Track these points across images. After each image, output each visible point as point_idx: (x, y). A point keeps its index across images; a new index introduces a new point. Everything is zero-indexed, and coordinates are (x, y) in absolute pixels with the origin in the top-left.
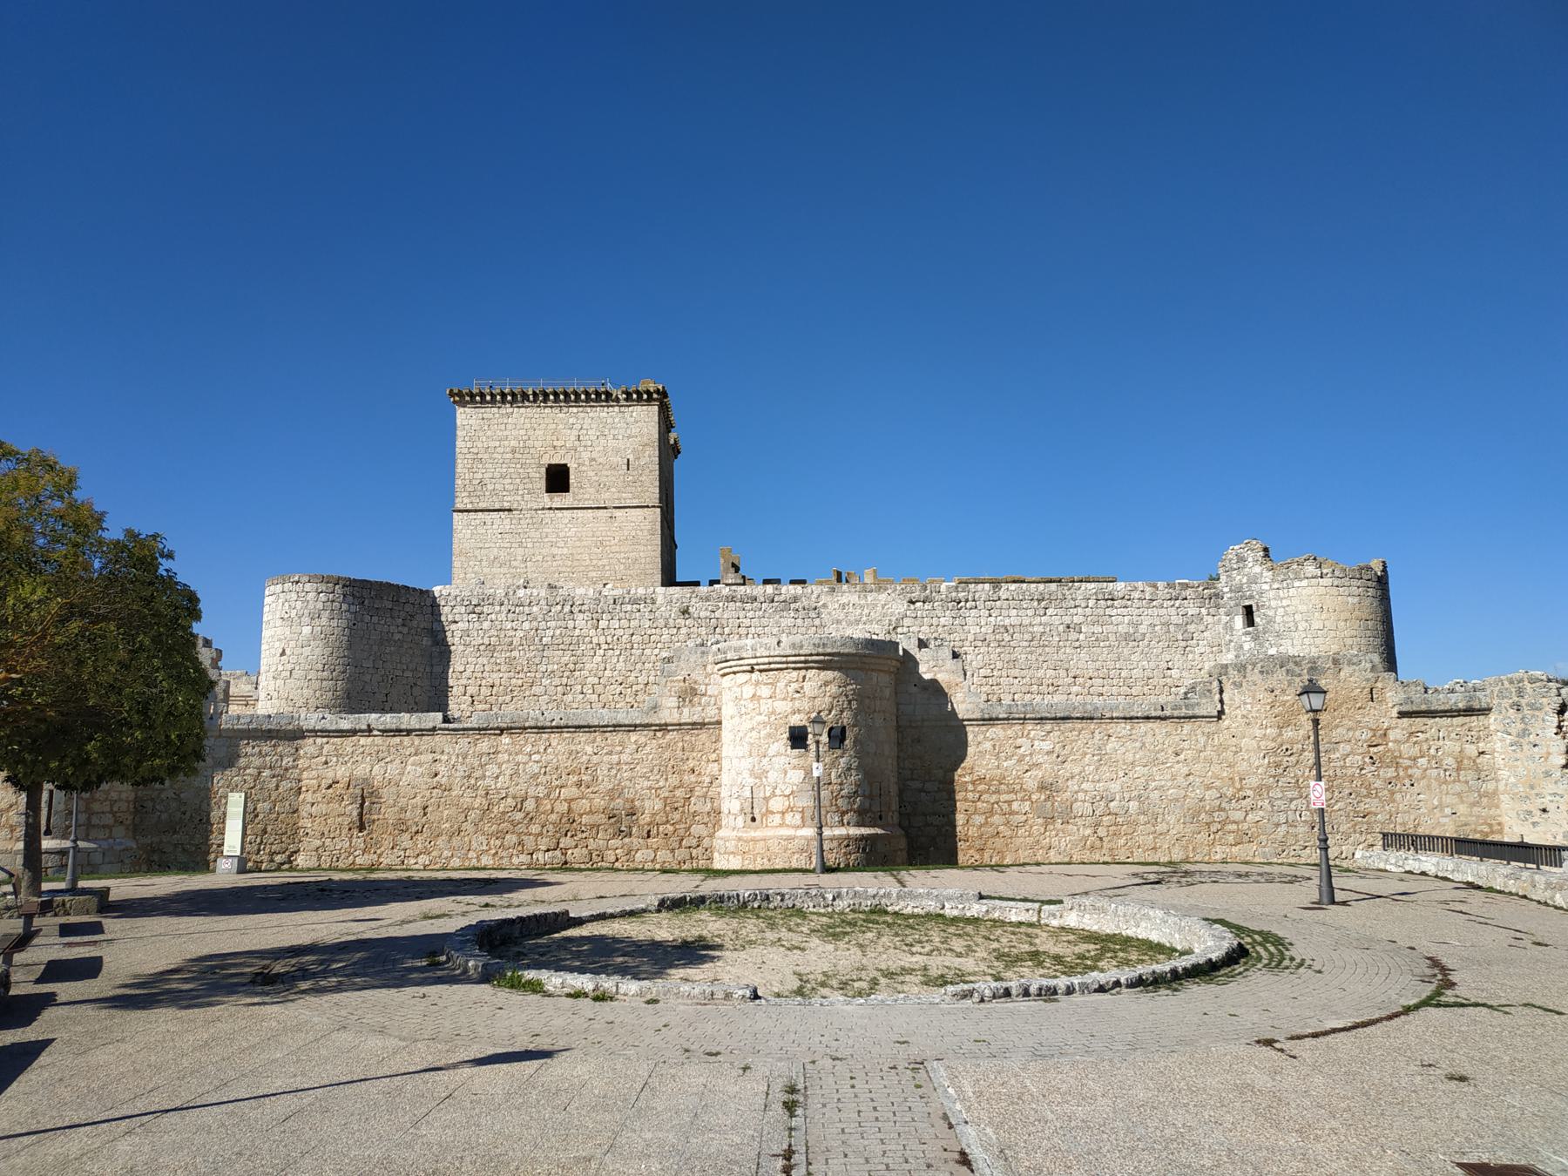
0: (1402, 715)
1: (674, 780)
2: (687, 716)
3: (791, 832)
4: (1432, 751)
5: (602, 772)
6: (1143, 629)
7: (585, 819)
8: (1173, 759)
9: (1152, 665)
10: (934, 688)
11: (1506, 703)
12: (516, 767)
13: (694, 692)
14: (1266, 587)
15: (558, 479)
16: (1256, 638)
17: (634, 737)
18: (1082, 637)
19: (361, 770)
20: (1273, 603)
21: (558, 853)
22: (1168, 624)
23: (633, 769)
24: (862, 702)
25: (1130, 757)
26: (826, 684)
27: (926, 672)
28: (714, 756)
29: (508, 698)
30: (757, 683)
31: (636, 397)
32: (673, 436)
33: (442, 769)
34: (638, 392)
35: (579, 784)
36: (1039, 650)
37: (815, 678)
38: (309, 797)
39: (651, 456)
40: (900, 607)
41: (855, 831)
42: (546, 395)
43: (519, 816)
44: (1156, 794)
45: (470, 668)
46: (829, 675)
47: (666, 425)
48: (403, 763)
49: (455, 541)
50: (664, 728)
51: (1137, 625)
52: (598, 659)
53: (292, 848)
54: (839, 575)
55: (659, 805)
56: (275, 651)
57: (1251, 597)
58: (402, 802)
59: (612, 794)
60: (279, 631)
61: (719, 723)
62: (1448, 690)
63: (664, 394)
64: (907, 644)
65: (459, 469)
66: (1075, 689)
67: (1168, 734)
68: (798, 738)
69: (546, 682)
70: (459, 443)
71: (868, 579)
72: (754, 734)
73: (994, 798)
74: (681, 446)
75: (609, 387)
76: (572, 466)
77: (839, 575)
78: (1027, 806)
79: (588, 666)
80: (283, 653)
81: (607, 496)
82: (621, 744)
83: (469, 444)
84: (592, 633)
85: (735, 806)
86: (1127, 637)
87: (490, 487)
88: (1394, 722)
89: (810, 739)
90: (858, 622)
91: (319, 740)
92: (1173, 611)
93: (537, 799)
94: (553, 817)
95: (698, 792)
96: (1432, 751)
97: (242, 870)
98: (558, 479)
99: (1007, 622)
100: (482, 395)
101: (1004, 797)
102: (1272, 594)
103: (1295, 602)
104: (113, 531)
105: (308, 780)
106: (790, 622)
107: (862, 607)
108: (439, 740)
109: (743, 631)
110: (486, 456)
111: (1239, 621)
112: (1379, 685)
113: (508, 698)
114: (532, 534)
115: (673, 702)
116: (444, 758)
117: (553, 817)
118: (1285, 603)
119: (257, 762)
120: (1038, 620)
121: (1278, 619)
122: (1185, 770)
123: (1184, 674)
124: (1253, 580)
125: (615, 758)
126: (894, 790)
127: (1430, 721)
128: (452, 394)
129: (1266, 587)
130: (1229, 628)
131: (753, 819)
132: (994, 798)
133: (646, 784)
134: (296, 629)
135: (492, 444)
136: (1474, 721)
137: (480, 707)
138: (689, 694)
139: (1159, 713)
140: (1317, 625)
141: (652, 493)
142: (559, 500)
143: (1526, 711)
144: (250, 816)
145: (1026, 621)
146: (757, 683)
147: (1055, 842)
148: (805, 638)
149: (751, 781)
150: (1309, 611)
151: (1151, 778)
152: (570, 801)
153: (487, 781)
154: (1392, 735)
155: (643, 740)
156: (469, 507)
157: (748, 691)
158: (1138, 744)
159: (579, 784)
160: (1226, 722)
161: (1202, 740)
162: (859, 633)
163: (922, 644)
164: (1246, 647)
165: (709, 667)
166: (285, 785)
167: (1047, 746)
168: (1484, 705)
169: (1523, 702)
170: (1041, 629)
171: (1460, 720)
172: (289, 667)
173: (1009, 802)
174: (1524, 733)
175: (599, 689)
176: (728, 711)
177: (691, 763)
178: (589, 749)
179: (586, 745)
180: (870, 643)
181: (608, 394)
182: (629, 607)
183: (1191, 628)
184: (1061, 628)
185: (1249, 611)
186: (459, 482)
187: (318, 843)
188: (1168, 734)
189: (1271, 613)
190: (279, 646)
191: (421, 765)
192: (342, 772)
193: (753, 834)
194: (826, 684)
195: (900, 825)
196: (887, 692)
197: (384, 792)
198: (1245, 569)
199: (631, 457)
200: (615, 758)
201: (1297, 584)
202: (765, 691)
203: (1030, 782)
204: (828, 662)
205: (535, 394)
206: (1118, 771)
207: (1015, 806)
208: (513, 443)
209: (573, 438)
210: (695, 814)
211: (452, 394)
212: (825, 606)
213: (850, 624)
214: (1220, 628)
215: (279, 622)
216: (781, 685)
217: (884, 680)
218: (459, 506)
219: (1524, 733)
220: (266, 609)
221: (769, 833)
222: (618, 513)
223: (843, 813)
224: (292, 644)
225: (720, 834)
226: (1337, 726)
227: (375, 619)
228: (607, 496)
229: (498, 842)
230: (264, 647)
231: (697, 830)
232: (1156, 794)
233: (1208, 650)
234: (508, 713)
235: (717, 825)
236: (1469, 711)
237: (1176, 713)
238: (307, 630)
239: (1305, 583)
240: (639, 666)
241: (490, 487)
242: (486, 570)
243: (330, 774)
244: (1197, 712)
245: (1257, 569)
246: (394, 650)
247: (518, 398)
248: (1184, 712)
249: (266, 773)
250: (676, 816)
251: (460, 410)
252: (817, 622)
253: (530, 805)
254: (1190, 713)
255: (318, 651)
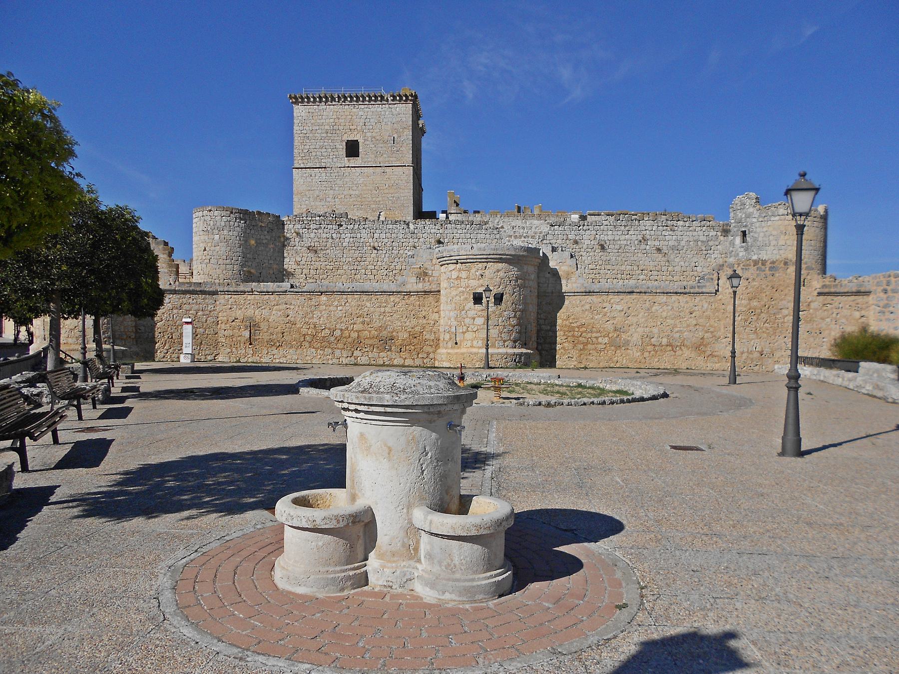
0: (820, 294)
1: (414, 322)
2: (420, 287)
3: (474, 350)
4: (834, 315)
5: (375, 317)
6: (683, 243)
7: (367, 342)
8: (688, 316)
9: (687, 264)
10: (555, 274)
11: (880, 289)
12: (330, 313)
13: (426, 274)
14: (755, 220)
15: (352, 149)
16: (746, 250)
17: (392, 298)
18: (648, 247)
19: (250, 312)
20: (758, 230)
21: (353, 358)
22: (697, 241)
23: (396, 318)
24: (522, 281)
25: (664, 314)
26: (498, 271)
27: (552, 264)
28: (436, 310)
29: (325, 276)
30: (460, 270)
31: (399, 98)
32: (421, 122)
33: (290, 313)
34: (400, 96)
35: (363, 323)
36: (623, 255)
37: (493, 267)
38: (223, 326)
39: (408, 134)
40: (545, 228)
41: (517, 351)
42: (345, 98)
43: (332, 339)
44: (677, 335)
45: (304, 259)
46: (500, 265)
47: (416, 115)
48: (266, 306)
49: (295, 186)
50: (409, 293)
51: (678, 241)
52: (373, 255)
53: (215, 352)
54: (519, 208)
55: (406, 335)
56: (199, 248)
57: (746, 226)
58: (271, 330)
59: (380, 329)
60: (202, 237)
61: (439, 291)
62: (848, 283)
63: (416, 97)
64: (545, 249)
65: (296, 143)
66: (642, 277)
67: (687, 302)
68: (478, 299)
69: (345, 267)
70: (296, 128)
71: (536, 212)
72: (458, 297)
73: (589, 335)
74: (427, 129)
75: (383, 92)
76: (361, 141)
77: (519, 208)
78: (606, 340)
79: (368, 259)
80: (205, 250)
81: (381, 159)
82: (386, 302)
83: (301, 128)
84: (370, 240)
85: (447, 337)
86: (673, 248)
87: (314, 154)
88: (814, 298)
89: (484, 300)
90: (520, 237)
91: (226, 296)
92: (701, 233)
93: (341, 330)
94: (350, 340)
95: (428, 328)
96: (834, 315)
97: (193, 361)
98: (352, 149)
99: (606, 238)
100: (308, 98)
101: (594, 335)
102: (758, 224)
103: (771, 229)
104: (34, 321)
105: (222, 317)
106: (483, 236)
107: (523, 228)
108: (288, 297)
109: (455, 241)
110: (311, 135)
111: (738, 240)
112: (809, 277)
113: (325, 276)
114: (338, 182)
115: (414, 280)
116: (292, 307)
117: (350, 340)
118: (765, 230)
119: (196, 307)
120: (623, 237)
121: (760, 239)
122: (694, 322)
123: (705, 269)
124: (748, 216)
125: (382, 310)
126: (534, 330)
127: (835, 298)
128: (291, 97)
129: (755, 220)
130: (732, 243)
131: (456, 343)
132: (589, 335)
133: (399, 324)
134: (211, 236)
135: (315, 128)
136: (860, 299)
137: (310, 281)
138: (423, 275)
139: (683, 291)
140: (781, 242)
141: (408, 158)
142: (354, 162)
143: (890, 294)
144: (195, 335)
145: (617, 238)
146: (460, 270)
147: (620, 359)
148: (484, 245)
149: (455, 323)
150: (773, 233)
151: (675, 326)
152: (358, 331)
153: (315, 320)
154: (813, 305)
155: (397, 300)
156: (302, 166)
157: (455, 275)
158: (670, 308)
159: (363, 323)
160: (719, 296)
161: (706, 305)
162: (518, 243)
163: (554, 250)
164: (741, 254)
165: (434, 261)
166: (210, 320)
167: (619, 307)
168: (867, 290)
169: (889, 288)
170: (625, 242)
171: (853, 298)
172: (208, 257)
173: (597, 338)
174: (886, 306)
175: (374, 272)
176: (444, 285)
177: (424, 313)
178: (368, 304)
179: (368, 304)
180: (529, 250)
181: (382, 97)
182: (391, 226)
183: (711, 243)
184: (636, 242)
185: (744, 234)
186: (296, 151)
187: (229, 350)
188: (687, 302)
189: (756, 235)
190: (202, 246)
191: (280, 311)
192: (239, 314)
193: (456, 351)
194: (498, 271)
195: (537, 349)
196: (533, 277)
197: (262, 325)
198: (744, 206)
199: (396, 136)
200: (382, 310)
201: (773, 218)
202: (464, 274)
203: (609, 326)
204: (513, 260)
205: (339, 97)
206: (640, 321)
207: (600, 340)
208: (327, 127)
209: (361, 124)
210: (426, 340)
211: (291, 97)
212: (502, 227)
213: (516, 237)
214: (728, 244)
215: (202, 233)
216: (473, 271)
217: (531, 269)
218: (296, 165)
219: (886, 306)
220: (194, 225)
221: (463, 350)
222: (388, 170)
223: (505, 341)
224: (209, 245)
225: (439, 351)
226: (782, 300)
227: (253, 232)
228: (381, 159)
229: (322, 352)
230: (194, 246)
231: (427, 349)
232: (677, 335)
233: (719, 256)
234: (326, 284)
235: (437, 346)
236: (858, 293)
237: (692, 291)
238: (217, 237)
239: (777, 218)
240: (397, 260)
241: (314, 154)
242: (313, 204)
243: (234, 315)
244: (704, 290)
245: (751, 210)
246: (262, 249)
247: (328, 99)
248: (697, 290)
249: (200, 313)
250: (415, 341)
251: (295, 107)
252: (498, 236)
253: (338, 333)
254: (700, 291)
255: (223, 249)
